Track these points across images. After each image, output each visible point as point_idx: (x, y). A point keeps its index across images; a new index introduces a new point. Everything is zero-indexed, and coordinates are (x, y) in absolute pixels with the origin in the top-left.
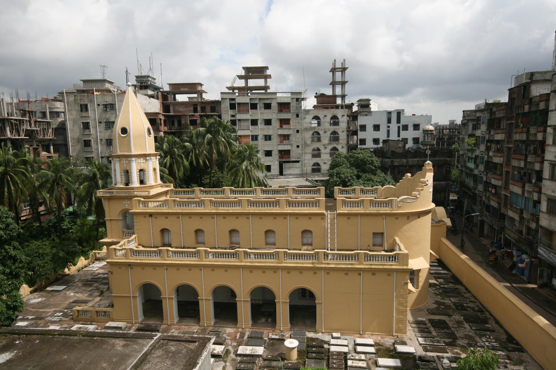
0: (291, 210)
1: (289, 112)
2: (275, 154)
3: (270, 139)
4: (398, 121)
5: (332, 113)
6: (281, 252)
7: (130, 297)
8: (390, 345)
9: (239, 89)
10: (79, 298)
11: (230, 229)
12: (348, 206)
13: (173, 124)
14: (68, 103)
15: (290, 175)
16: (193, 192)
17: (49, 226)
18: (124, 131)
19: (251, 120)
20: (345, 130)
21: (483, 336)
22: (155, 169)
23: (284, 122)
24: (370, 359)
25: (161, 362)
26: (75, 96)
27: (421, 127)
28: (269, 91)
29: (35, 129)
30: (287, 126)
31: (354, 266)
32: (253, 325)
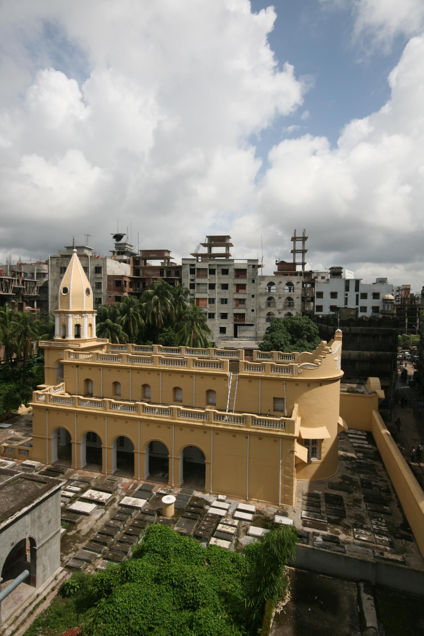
0: (197, 369)
1: (245, 277)
2: (230, 317)
3: (226, 303)
4: (357, 289)
5: (287, 279)
6: (175, 408)
7: (46, 439)
8: (271, 515)
9: (203, 255)
10: (16, 436)
11: (143, 383)
12: (250, 369)
13: (139, 286)
14: (51, 266)
15: (244, 337)
16: (152, 349)
17: (21, 371)
18: (65, 290)
19: (209, 284)
20: (300, 296)
21: (377, 518)
22: (90, 325)
23: (240, 287)
24: (243, 526)
25: (4, 498)
26: (57, 260)
27: (381, 296)
28: (230, 258)
29: (22, 287)
30: (243, 290)
31: (241, 429)
32: (149, 479)
